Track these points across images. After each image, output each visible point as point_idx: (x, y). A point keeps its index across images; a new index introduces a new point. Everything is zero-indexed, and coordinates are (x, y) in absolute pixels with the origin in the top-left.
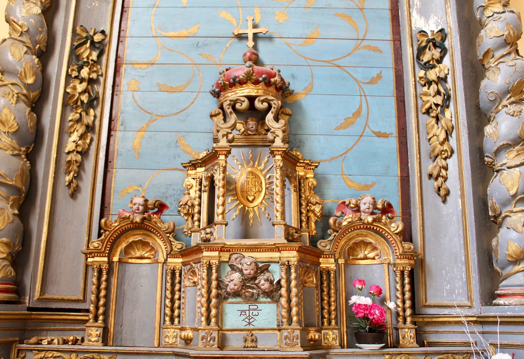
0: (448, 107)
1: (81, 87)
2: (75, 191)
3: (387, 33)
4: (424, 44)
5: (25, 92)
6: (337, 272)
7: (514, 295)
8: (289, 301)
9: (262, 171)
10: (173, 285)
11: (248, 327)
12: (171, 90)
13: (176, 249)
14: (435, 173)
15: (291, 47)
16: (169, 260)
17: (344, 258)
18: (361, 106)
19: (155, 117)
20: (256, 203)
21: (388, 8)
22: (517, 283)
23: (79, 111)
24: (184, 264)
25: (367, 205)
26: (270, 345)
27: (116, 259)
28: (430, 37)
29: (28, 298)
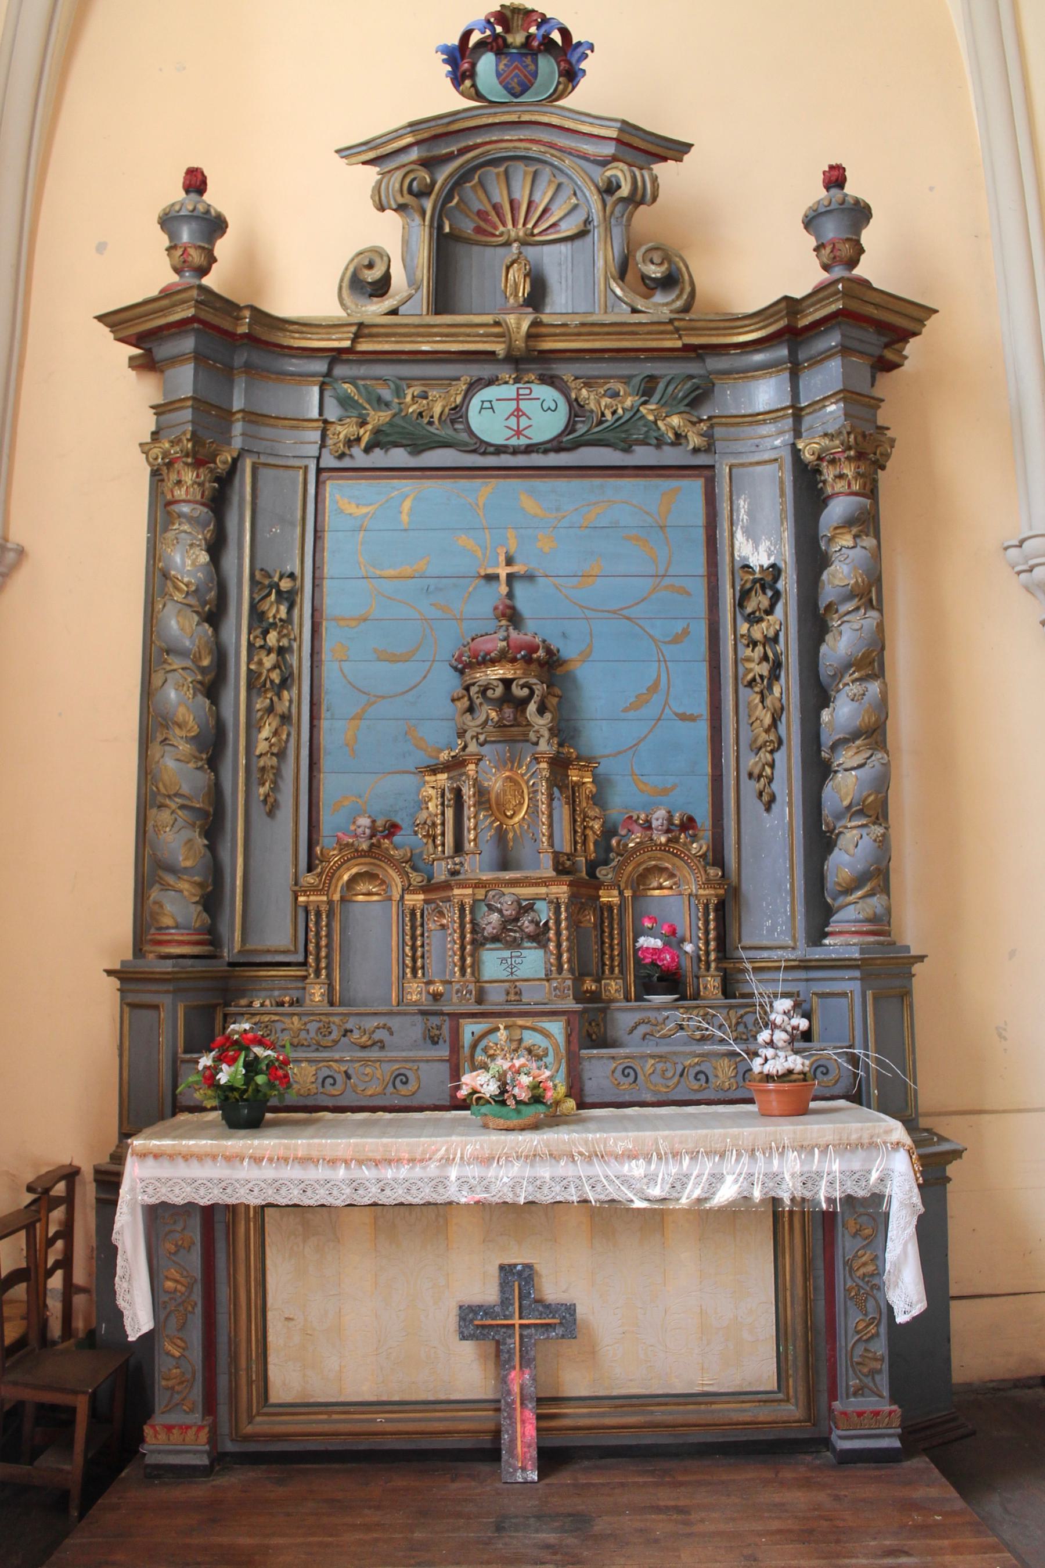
0: (777, 678)
1: (269, 661)
2: (272, 806)
3: (699, 564)
4: (748, 586)
5: (199, 677)
6: (622, 906)
7: (840, 933)
8: (559, 946)
9: (522, 775)
10: (413, 928)
11: (510, 977)
12: (393, 659)
13: (415, 883)
14: (756, 772)
15: (561, 591)
16: (407, 897)
17: (632, 888)
18: (659, 676)
19: (374, 699)
20: (516, 819)
21: (701, 524)
22: (846, 918)
23: (269, 695)
24: (426, 902)
25: (660, 821)
26: (537, 998)
27: (337, 897)
28: (758, 576)
29: (226, 950)
